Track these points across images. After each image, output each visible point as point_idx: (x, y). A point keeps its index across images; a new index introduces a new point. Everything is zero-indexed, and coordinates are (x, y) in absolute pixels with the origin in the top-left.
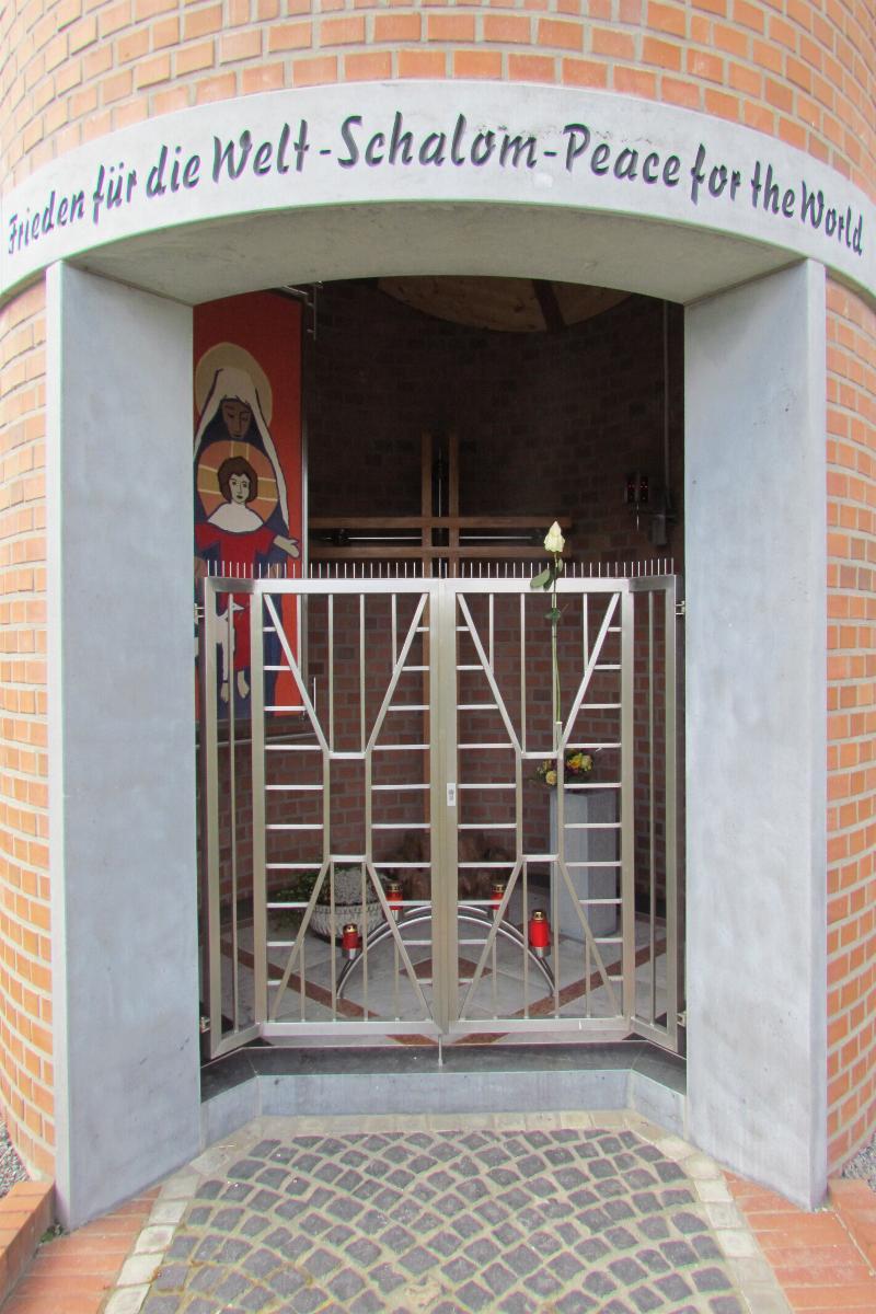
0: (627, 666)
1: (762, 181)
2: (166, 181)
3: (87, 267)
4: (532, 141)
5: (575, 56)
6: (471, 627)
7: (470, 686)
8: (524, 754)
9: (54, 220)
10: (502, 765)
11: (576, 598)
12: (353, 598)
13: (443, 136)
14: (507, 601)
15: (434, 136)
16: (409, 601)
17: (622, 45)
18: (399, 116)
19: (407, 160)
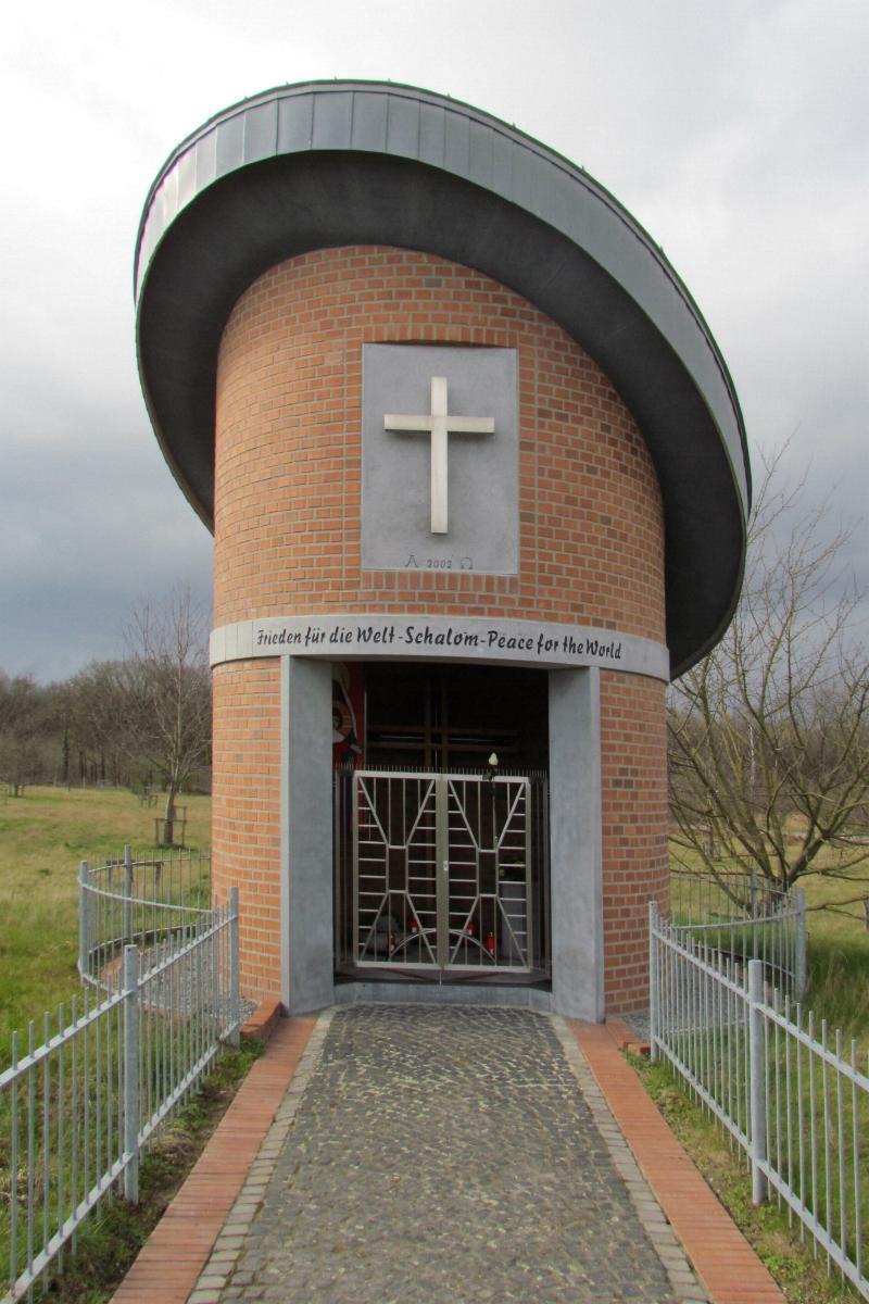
0: (528, 814)
1: (568, 643)
2: (338, 638)
3: (298, 659)
6: (455, 795)
7: (455, 820)
8: (479, 850)
9: (286, 639)
10: (470, 854)
11: (503, 785)
12: (400, 780)
14: (472, 785)
16: (425, 783)
17: (512, 602)
18: (427, 629)
19: (430, 642)
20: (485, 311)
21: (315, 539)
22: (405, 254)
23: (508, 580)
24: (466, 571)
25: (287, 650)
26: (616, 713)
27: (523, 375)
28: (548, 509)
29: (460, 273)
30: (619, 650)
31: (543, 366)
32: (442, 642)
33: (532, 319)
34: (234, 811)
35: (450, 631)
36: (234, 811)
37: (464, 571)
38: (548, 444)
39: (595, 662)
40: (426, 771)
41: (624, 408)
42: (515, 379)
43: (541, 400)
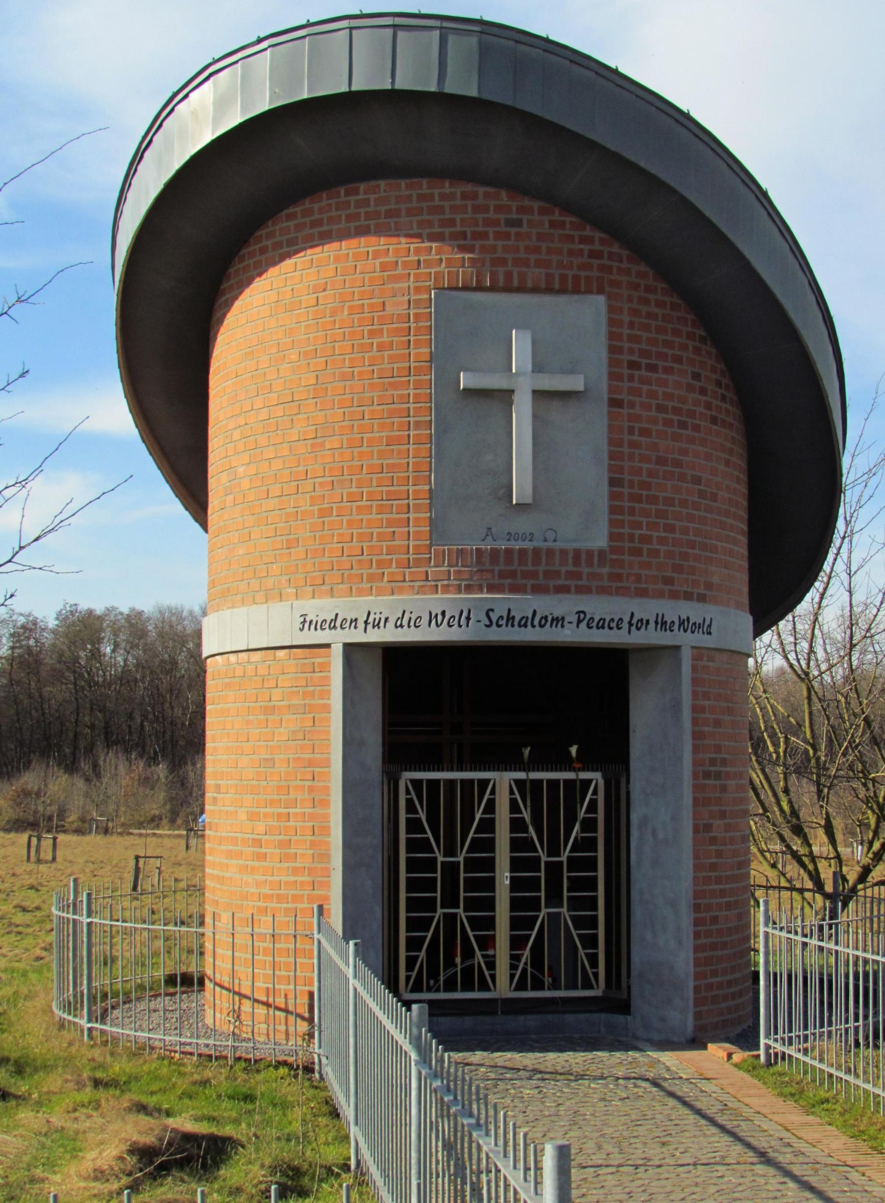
2: (405, 622)
4: (563, 618)
5: (580, 583)
6: (518, 796)
7: (517, 825)
9: (338, 624)
13: (527, 618)
15: (523, 618)
16: (484, 783)
18: (509, 610)
19: (513, 626)
20: (571, 253)
21: (374, 510)
22: (481, 190)
23: (596, 554)
24: (550, 544)
25: (338, 638)
26: (706, 696)
27: (611, 322)
28: (638, 472)
29: (542, 212)
30: (710, 626)
31: (634, 312)
32: (525, 626)
33: (621, 261)
34: (261, 826)
35: (535, 612)
36: (261, 826)
37: (546, 544)
38: (638, 399)
39: (687, 640)
40: (443, 770)
41: (714, 351)
42: (604, 329)
43: (631, 351)
